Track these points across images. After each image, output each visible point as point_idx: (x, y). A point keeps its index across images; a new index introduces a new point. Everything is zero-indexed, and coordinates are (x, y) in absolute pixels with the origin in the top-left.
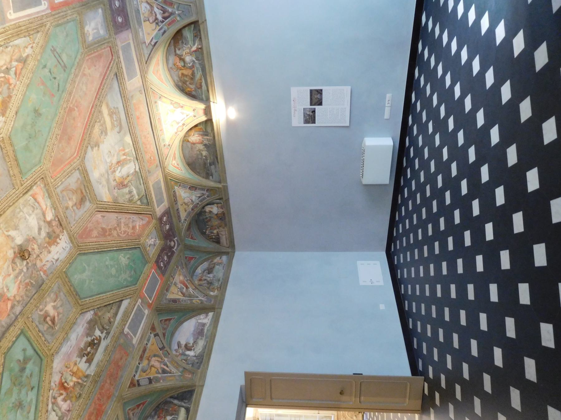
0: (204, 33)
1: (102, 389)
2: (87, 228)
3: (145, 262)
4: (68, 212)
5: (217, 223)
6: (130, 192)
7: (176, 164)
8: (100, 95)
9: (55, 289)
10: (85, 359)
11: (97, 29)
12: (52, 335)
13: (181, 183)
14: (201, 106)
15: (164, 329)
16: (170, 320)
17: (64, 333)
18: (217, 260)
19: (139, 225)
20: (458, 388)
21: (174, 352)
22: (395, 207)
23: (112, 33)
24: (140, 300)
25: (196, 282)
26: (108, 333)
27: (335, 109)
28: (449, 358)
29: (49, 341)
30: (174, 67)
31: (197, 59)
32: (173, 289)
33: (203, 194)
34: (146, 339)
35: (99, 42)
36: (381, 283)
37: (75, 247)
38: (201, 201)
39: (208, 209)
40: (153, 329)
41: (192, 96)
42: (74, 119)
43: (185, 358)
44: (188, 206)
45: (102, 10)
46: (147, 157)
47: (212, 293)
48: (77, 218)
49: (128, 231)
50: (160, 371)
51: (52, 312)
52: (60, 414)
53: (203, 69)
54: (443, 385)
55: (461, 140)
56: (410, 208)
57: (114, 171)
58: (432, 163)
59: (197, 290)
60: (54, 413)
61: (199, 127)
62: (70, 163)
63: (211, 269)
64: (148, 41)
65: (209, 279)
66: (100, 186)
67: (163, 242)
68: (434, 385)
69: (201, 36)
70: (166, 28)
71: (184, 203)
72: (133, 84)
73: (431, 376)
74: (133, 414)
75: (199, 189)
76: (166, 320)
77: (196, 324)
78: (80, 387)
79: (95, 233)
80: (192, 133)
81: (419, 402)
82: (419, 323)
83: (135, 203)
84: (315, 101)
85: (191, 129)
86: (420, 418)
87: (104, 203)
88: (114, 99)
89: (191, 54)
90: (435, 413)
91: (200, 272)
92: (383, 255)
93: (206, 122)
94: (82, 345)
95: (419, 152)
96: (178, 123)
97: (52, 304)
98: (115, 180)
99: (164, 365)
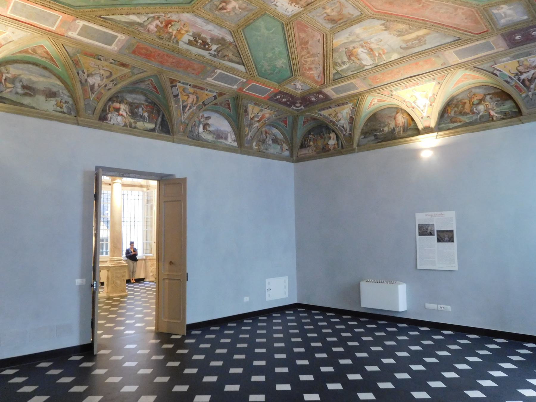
0: (506, 123)
1: (167, 56)
2: (307, 27)
3: (280, 82)
4: (321, 9)
5: (319, 144)
6: (344, 63)
7: (374, 103)
8: (435, 26)
9: (250, 7)
10: (192, 39)
11: (506, 16)
12: (210, 9)
13: (356, 109)
14: (432, 124)
15: (221, 104)
16: (229, 108)
17: (212, 19)
18: (285, 146)
19: (313, 74)
20: (177, 364)
21: (201, 114)
22: (339, 313)
23: (503, 32)
24: (245, 80)
25: (264, 129)
26: (214, 56)
27: (434, 256)
28: (202, 357)
29: (205, 8)
30: (472, 94)
31: (482, 117)
32: (257, 109)
33: (346, 131)
35: (491, 20)
36: (268, 299)
37: (289, 19)
38: (340, 129)
39: (333, 135)
40: (221, 94)
41: (443, 114)
42: (410, 5)
43: (197, 124)
44: (334, 117)
45: (527, 19)
46: (379, 75)
47: (254, 144)
48: (315, 18)
49: (307, 65)
51: (230, 7)
52: (146, 24)
53: (470, 124)
54: (180, 351)
55: (400, 376)
56: (337, 327)
57: (362, 47)
58: (379, 349)
60: (146, 19)
61: (412, 123)
62: (367, 5)
63: (277, 142)
64: (497, 66)
65: (267, 140)
66: (347, 35)
67: (299, 96)
68: (179, 343)
69: (506, 119)
70: (513, 83)
71: (337, 113)
72: (451, 56)
73: (187, 341)
74: (148, 84)
75: (351, 127)
76: (229, 105)
78: (168, 37)
79: (303, 35)
80: (406, 116)
81: (165, 331)
82: (232, 332)
83: (334, 68)
84: (441, 234)
85: (409, 115)
86: (151, 331)
87: (331, 40)
88: (433, 40)
89: (487, 110)
90: (156, 344)
91: (274, 132)
92: (294, 300)
93: (417, 129)
94: (203, 35)
95: (391, 336)
96: (414, 102)
97: (237, 6)
98: (354, 48)
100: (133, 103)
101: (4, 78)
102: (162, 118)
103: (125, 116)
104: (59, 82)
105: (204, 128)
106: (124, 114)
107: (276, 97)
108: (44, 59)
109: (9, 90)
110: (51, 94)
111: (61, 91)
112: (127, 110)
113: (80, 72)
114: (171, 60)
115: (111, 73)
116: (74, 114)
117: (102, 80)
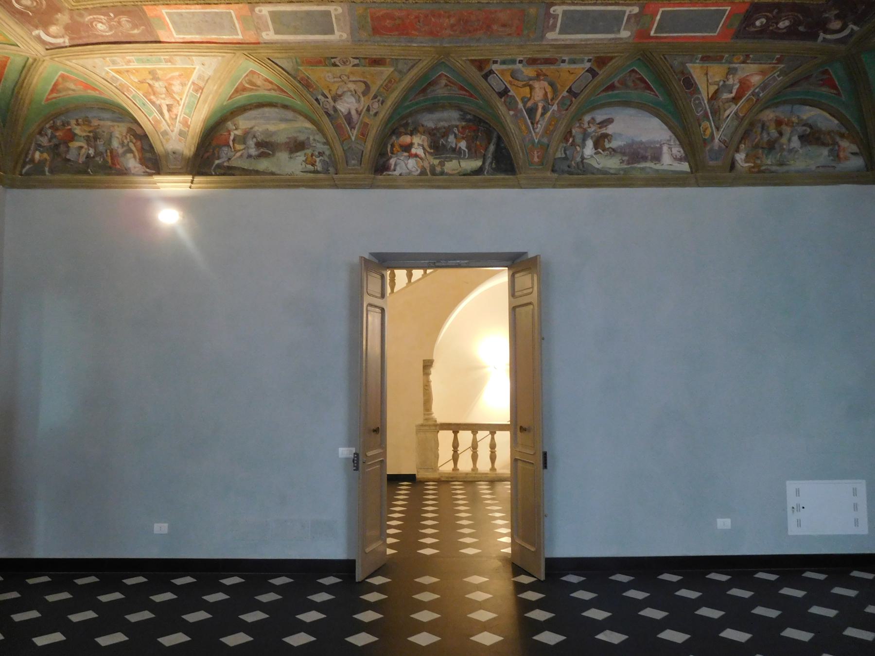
1: (434, 16)
15: (623, 83)
16: (648, 88)
24: (636, 10)
28: (831, 613)
32: (717, 71)
34: (573, 56)
36: (793, 530)
40: (602, 61)
43: (578, 140)
50: (529, 104)
59: (736, 123)
63: (818, 139)
76: (642, 80)
77: (658, 142)
99: (544, 108)
100: (436, 129)
101: (232, 138)
102: (498, 145)
103: (423, 155)
104: (308, 125)
105: (596, 145)
106: (420, 152)
107: (753, 24)
108: (273, 93)
109: (239, 154)
110: (296, 146)
111: (311, 138)
112: (426, 145)
113: (320, 97)
114: (446, 22)
115: (365, 83)
116: (331, 173)
117: (358, 101)
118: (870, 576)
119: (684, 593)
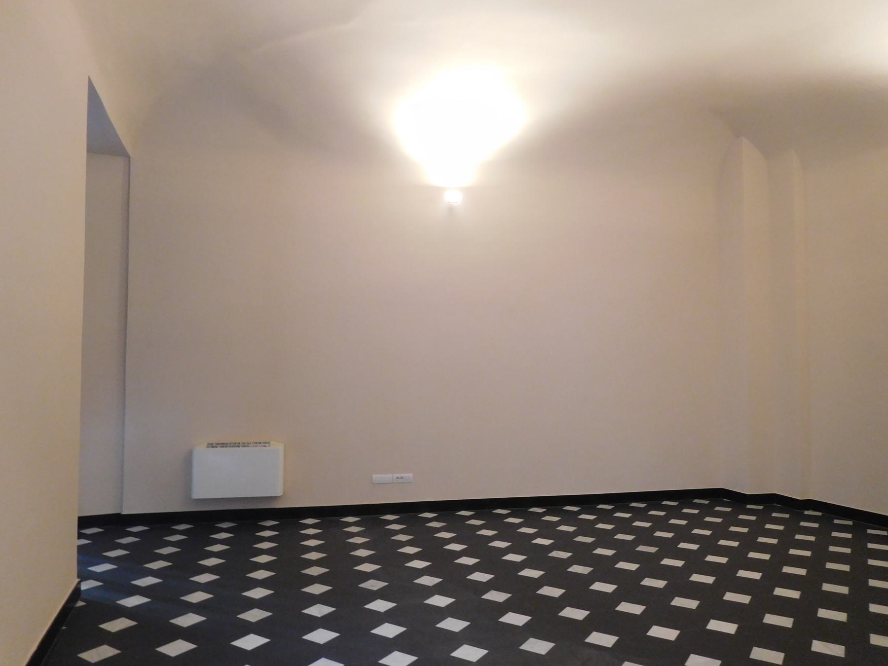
28: (679, 563)
118: (884, 533)
119: (539, 541)
